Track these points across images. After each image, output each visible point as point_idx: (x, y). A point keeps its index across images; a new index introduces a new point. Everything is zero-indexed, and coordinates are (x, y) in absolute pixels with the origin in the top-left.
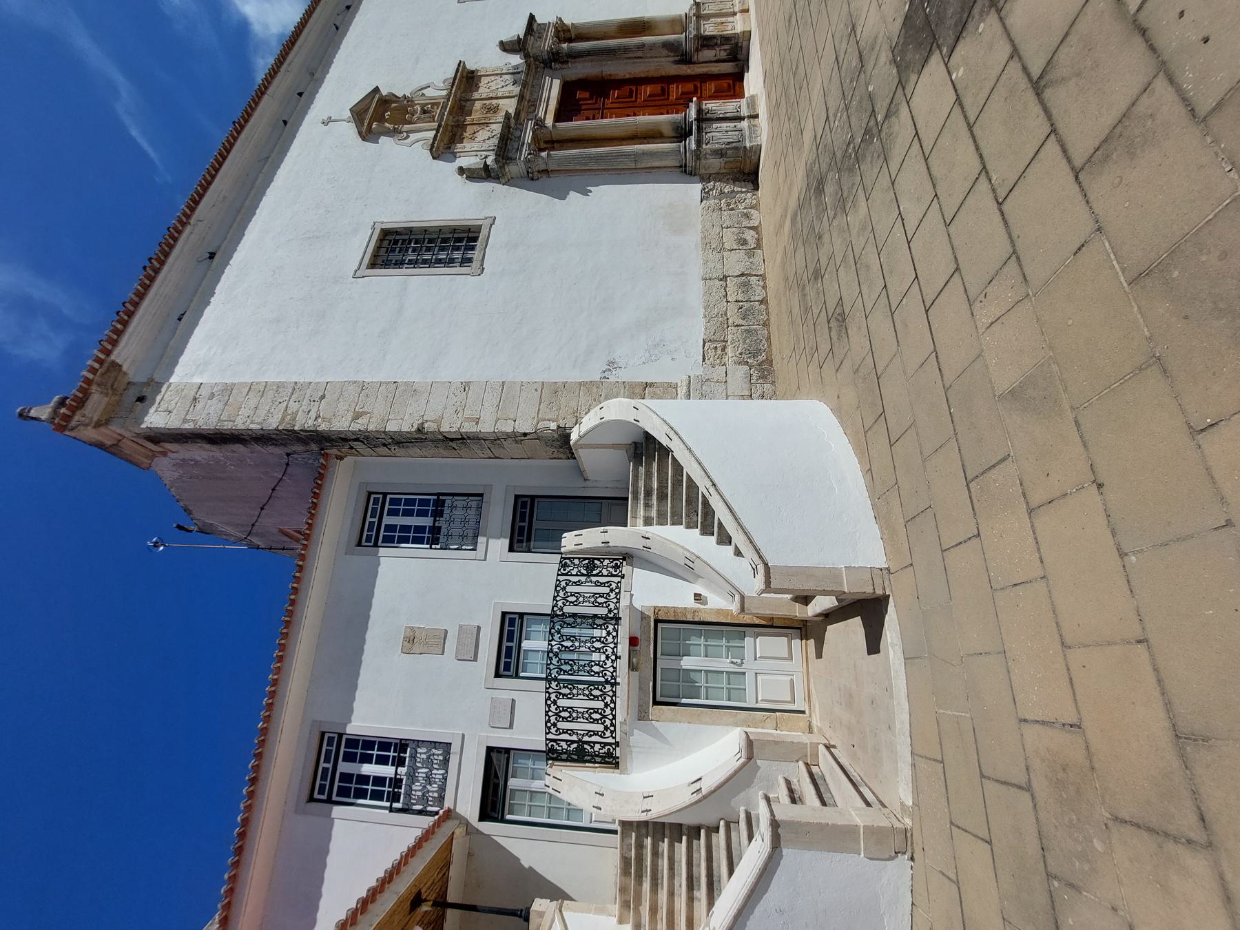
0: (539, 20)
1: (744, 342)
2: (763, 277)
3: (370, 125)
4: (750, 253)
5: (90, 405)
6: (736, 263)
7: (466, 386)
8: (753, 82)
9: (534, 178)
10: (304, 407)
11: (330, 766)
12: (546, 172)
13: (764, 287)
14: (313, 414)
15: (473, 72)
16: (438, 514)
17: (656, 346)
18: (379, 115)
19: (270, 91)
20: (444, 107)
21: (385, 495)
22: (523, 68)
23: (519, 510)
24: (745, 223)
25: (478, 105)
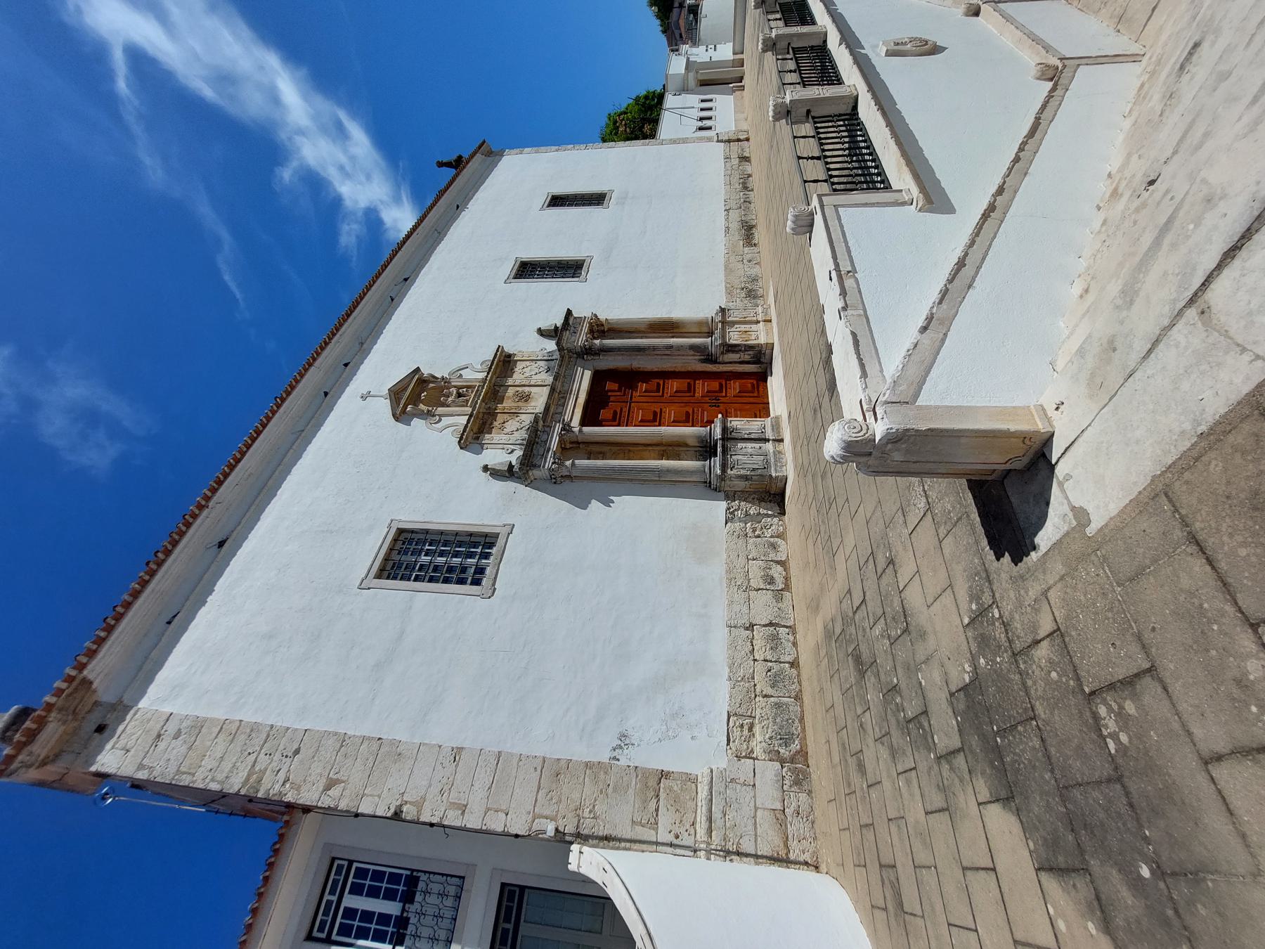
1: (775, 722)
2: (792, 629)
4: (778, 596)
5: (42, 737)
6: (762, 608)
7: (457, 752)
8: (776, 386)
9: (557, 483)
10: (274, 764)
11: (334, 898)
12: (569, 477)
13: (795, 644)
14: (282, 776)
15: (509, 356)
16: (408, 898)
17: (674, 716)
18: (416, 396)
19: (317, 363)
21: (351, 862)
22: (557, 356)
23: (505, 903)
24: (772, 556)
25: (511, 391)
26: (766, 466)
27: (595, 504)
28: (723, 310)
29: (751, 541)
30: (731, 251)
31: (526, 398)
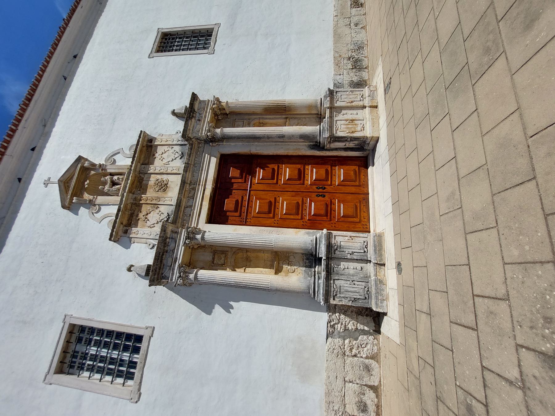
0: (201, 97)
3: (71, 199)
8: (379, 180)
18: (81, 184)
20: (129, 173)
24: (366, 380)
25: (153, 179)
26: (367, 297)
27: (218, 310)
28: (331, 93)
29: (349, 360)
30: (340, 14)
31: (163, 187)
